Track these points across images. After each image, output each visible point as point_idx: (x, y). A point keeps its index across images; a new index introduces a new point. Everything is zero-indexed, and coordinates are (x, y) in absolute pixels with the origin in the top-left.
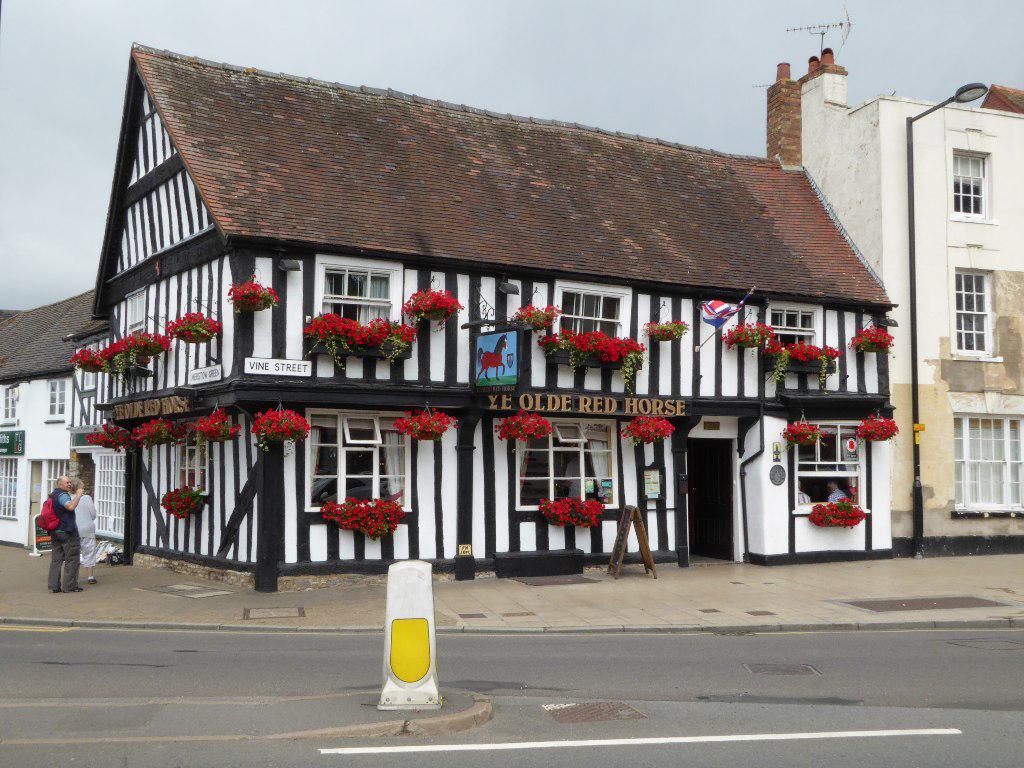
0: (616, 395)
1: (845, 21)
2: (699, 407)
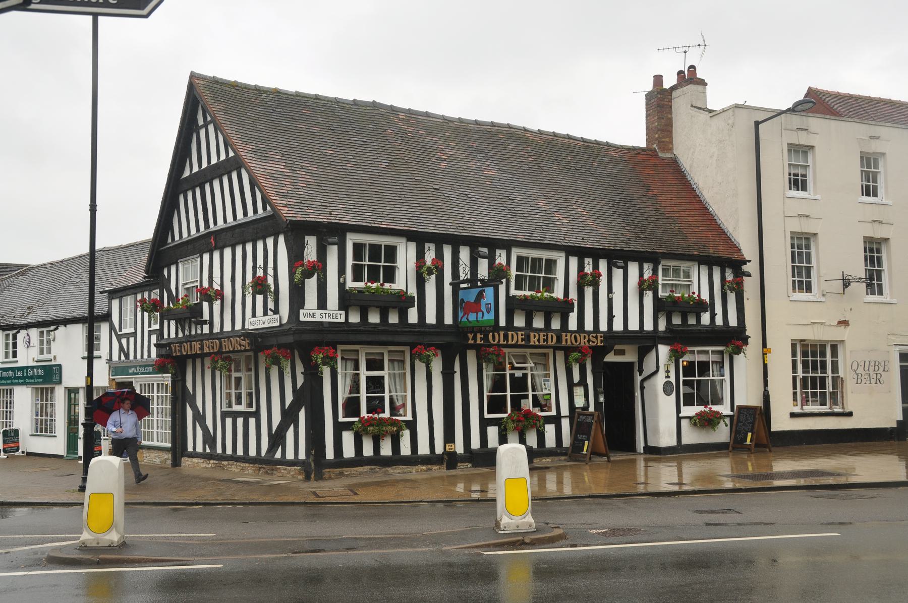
0: (555, 331)
1: (702, 43)
2: (613, 339)
